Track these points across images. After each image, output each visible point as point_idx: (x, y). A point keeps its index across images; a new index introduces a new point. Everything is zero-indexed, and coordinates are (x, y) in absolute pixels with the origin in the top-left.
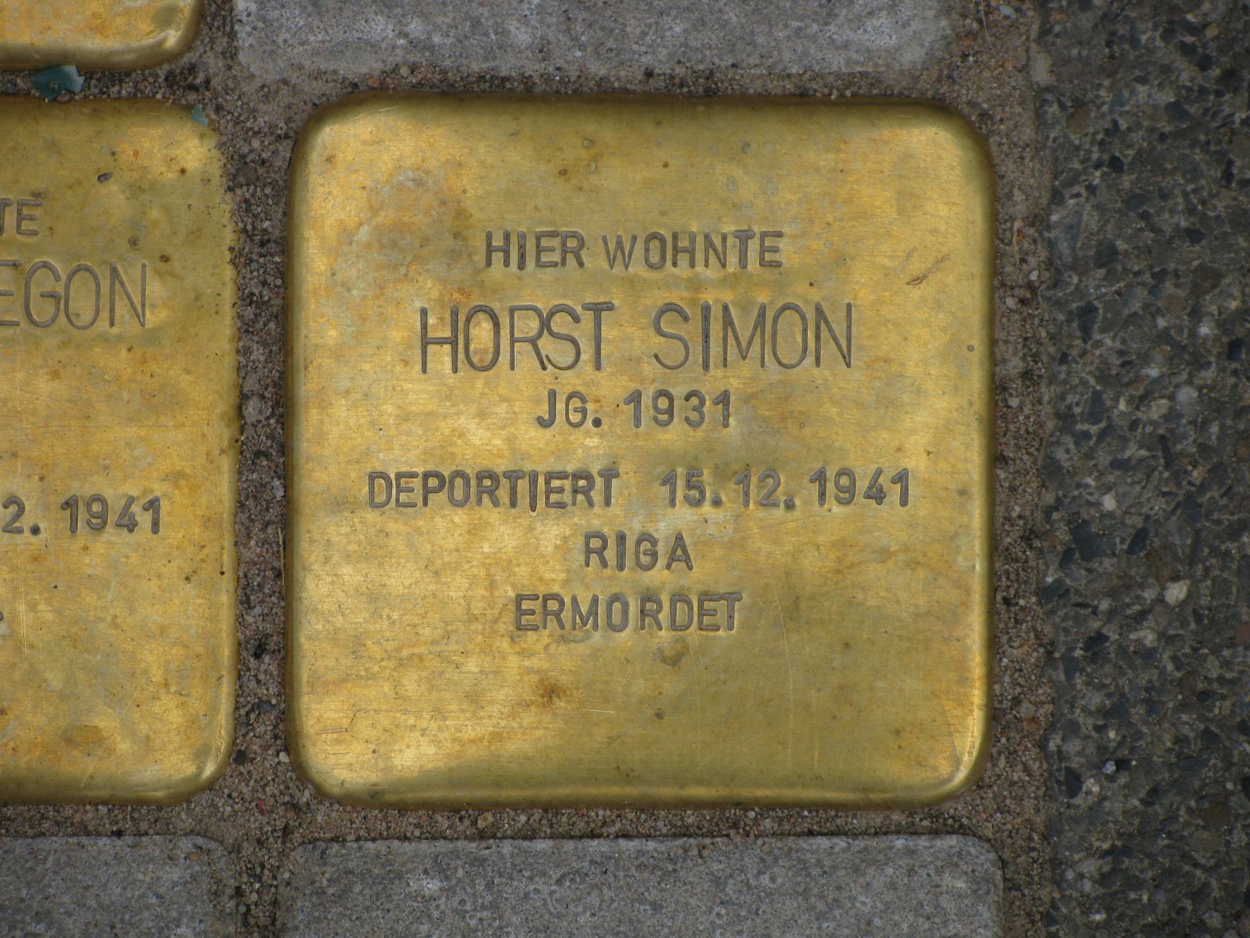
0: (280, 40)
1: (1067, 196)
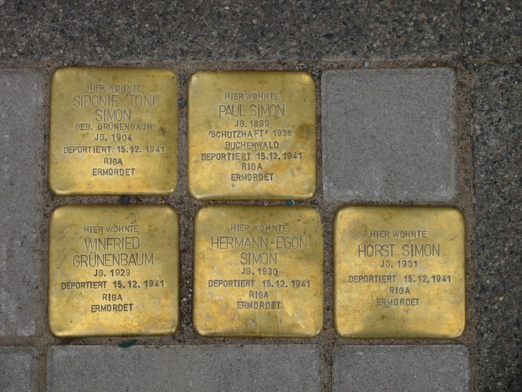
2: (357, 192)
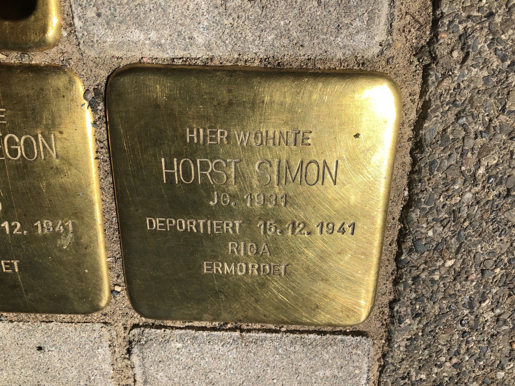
0: (95, 40)
1: (433, 116)
2: (153, 35)
